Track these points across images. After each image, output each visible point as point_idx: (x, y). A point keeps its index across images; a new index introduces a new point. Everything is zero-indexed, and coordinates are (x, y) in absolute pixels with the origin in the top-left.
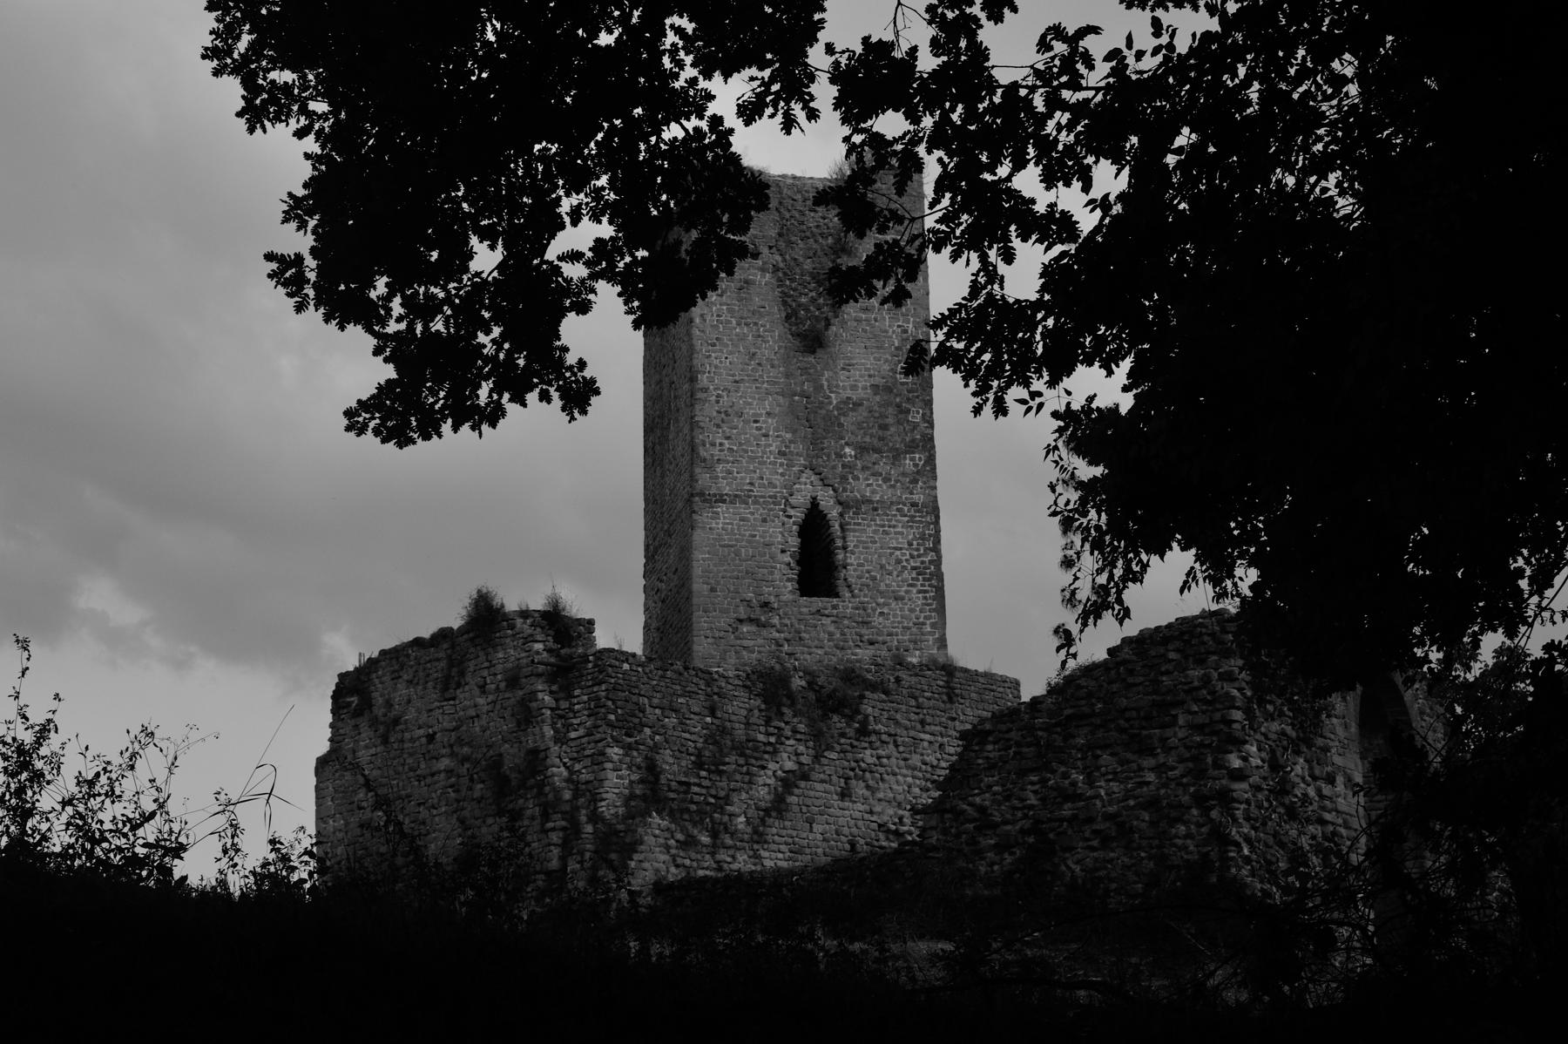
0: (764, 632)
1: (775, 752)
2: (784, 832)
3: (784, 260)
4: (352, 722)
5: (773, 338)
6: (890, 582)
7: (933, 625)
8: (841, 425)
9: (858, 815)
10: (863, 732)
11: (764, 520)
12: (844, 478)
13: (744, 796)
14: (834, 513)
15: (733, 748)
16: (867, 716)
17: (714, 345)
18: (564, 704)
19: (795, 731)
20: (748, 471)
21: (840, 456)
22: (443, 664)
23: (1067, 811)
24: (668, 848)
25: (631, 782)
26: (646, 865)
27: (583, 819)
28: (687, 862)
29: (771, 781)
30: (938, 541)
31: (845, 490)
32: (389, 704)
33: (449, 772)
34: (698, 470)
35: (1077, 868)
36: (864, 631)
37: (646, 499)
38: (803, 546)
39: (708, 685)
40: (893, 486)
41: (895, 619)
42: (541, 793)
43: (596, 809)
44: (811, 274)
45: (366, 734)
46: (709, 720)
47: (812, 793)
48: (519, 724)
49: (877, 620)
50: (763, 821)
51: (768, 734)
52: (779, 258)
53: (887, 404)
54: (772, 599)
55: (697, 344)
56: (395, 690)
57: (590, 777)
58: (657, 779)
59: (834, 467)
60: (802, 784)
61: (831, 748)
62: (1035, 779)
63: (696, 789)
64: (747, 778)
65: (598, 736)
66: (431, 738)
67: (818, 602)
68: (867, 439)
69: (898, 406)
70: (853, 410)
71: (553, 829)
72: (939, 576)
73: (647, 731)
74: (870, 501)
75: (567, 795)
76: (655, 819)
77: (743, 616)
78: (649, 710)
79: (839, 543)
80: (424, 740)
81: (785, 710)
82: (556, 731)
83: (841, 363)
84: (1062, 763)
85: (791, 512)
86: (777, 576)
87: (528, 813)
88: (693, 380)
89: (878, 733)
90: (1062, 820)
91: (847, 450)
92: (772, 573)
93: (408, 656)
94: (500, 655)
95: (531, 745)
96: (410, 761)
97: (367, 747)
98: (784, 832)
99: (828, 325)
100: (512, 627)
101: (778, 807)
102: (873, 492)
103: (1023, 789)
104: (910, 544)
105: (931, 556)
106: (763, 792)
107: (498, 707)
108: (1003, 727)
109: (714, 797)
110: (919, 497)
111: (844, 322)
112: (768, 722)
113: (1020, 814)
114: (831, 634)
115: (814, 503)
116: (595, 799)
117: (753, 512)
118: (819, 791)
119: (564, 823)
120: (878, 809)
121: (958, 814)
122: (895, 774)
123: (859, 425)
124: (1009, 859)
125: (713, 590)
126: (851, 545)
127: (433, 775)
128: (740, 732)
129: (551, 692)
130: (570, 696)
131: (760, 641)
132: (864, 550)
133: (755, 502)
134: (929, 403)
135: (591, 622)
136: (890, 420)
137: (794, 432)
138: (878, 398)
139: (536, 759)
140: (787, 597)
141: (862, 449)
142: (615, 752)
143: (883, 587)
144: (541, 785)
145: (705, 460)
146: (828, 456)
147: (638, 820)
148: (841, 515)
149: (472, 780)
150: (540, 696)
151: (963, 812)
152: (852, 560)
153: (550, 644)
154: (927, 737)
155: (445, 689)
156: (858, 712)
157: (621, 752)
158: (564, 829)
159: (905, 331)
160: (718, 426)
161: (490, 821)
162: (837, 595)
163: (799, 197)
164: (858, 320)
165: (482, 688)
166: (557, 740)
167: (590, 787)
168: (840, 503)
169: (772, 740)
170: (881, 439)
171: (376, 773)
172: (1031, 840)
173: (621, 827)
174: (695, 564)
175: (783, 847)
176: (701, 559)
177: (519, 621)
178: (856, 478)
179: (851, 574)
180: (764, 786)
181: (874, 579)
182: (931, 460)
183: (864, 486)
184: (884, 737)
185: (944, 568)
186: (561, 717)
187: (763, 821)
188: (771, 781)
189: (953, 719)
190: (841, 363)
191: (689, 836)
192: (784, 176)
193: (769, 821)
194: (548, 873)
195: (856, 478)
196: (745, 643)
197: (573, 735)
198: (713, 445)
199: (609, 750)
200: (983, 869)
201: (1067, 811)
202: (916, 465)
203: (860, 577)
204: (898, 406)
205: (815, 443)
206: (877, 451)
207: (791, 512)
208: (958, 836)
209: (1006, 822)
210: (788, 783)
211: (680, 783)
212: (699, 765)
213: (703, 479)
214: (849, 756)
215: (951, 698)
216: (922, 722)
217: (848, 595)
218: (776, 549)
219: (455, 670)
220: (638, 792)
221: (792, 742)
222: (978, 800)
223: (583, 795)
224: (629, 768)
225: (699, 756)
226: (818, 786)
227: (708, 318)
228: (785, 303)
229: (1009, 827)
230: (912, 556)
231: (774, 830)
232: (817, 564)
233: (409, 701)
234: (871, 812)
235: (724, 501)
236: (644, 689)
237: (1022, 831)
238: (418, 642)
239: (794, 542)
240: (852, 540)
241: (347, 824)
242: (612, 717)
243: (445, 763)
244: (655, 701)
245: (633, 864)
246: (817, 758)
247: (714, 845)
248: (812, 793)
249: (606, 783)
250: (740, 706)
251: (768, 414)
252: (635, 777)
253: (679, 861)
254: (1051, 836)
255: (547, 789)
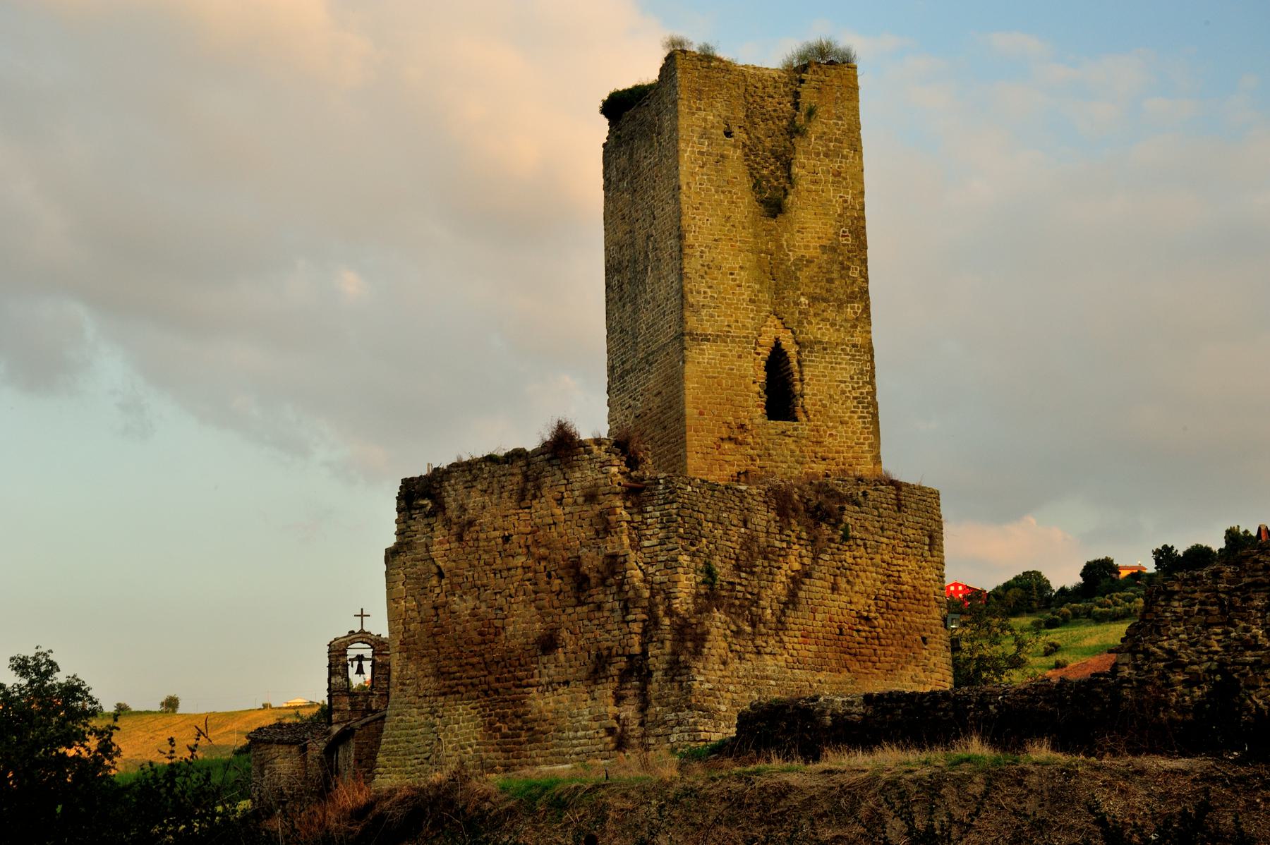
0: (741, 449)
1: (785, 556)
2: (797, 621)
3: (750, 138)
4: (426, 521)
5: (745, 205)
6: (836, 409)
7: (871, 445)
8: (797, 279)
9: (843, 605)
10: (845, 538)
11: (740, 357)
12: (800, 323)
13: (769, 592)
14: (792, 351)
15: (760, 553)
16: (847, 525)
17: (697, 209)
18: (638, 518)
19: (799, 538)
20: (726, 315)
21: (797, 304)
22: (519, 478)
23: (1249, 657)
24: (725, 636)
25: (697, 584)
26: (713, 651)
27: (661, 613)
28: (738, 648)
29: (784, 579)
30: (873, 376)
31: (801, 332)
32: (463, 508)
33: (526, 568)
34: (687, 314)
35: (1261, 703)
36: (818, 449)
37: (610, 330)
38: (769, 378)
39: (741, 502)
40: (838, 330)
41: (842, 440)
42: (620, 589)
43: (670, 605)
44: (771, 151)
45: (440, 532)
46: (743, 530)
47: (814, 589)
48: (597, 532)
49: (828, 441)
50: (783, 612)
51: (782, 541)
52: (745, 136)
53: (832, 262)
54: (747, 422)
55: (685, 207)
56: (468, 497)
57: (665, 579)
58: (714, 579)
59: (792, 313)
60: (807, 581)
61: (825, 552)
62: (1219, 631)
63: (739, 588)
64: (770, 578)
65: (670, 546)
66: (506, 539)
67: (783, 425)
68: (818, 291)
69: (841, 263)
70: (806, 266)
71: (635, 621)
72: (875, 406)
73: (704, 540)
74: (820, 342)
75: (647, 594)
76: (718, 615)
77: (725, 436)
78: (705, 524)
79: (797, 376)
80: (500, 541)
81: (793, 521)
82: (632, 540)
83: (796, 227)
84: (1242, 619)
85: (760, 350)
86: (751, 403)
87: (608, 606)
88: (681, 237)
89: (854, 538)
90: (1244, 664)
91: (803, 299)
92: (746, 400)
93: (481, 469)
94: (578, 475)
95: (610, 551)
96: (485, 556)
97: (441, 543)
98: (797, 621)
99: (786, 194)
100: (590, 452)
101: (792, 600)
102: (823, 335)
103: (1208, 638)
104: (852, 378)
105: (868, 388)
106: (779, 587)
107: (576, 517)
108: (1188, 589)
109: (751, 594)
110: (858, 340)
111: (798, 192)
112: (781, 532)
113: (1205, 658)
114: (793, 452)
115: (777, 343)
116: (669, 597)
117: (731, 350)
118: (816, 587)
119: (644, 616)
120: (855, 600)
121: (1148, 655)
122: (865, 571)
123: (811, 279)
124: (1198, 692)
125: (701, 414)
126: (807, 378)
127: (509, 569)
128: (762, 539)
129: (626, 508)
130: (641, 512)
131: (739, 457)
132: (817, 382)
133: (733, 342)
134: (864, 262)
135: (561, 427)
136: (835, 275)
137: (761, 283)
138: (825, 257)
139: (614, 563)
140: (758, 421)
141: (814, 299)
142: (684, 559)
143: (831, 414)
144: (620, 585)
145: (692, 306)
146: (788, 304)
147: (705, 615)
148: (798, 353)
149: (549, 576)
150: (618, 510)
151: (1154, 653)
152: (807, 390)
153: (624, 468)
154: (885, 540)
155: (522, 498)
156: (841, 521)
157: (688, 558)
158: (644, 621)
159: (846, 201)
160: (702, 277)
161: (570, 610)
162: (796, 419)
163: (759, 85)
164: (809, 191)
165: (560, 501)
166: (633, 547)
167: (664, 586)
168: (797, 343)
169: (784, 545)
170: (828, 291)
171: (450, 565)
172: (1218, 678)
173: (693, 621)
174: (687, 392)
175: (798, 634)
176: (692, 388)
177: (595, 448)
178: (810, 323)
179: (808, 401)
180: (779, 588)
181: (824, 406)
182: (867, 309)
183: (815, 330)
184: (859, 542)
185: (878, 398)
186: (634, 528)
187: (783, 612)
188: (784, 579)
189: (900, 525)
190: (796, 227)
191: (738, 626)
192: (746, 66)
193: (788, 612)
194: (631, 657)
195: (810, 323)
196: (728, 458)
197: (646, 543)
198: (699, 292)
199: (680, 558)
200: (1174, 699)
201: (1249, 657)
202: (855, 313)
203: (814, 405)
204: (841, 263)
205: (778, 292)
206: (826, 300)
207: (760, 350)
208: (1150, 671)
209: (1194, 663)
210: (797, 581)
211: (729, 583)
212: (738, 567)
213: (691, 322)
214: (837, 557)
215: (900, 507)
216: (882, 528)
217: (805, 419)
218: (749, 381)
219: (530, 485)
220: (703, 592)
221: (796, 547)
222: (1166, 644)
223: (658, 593)
224: (695, 572)
225: (737, 560)
226: (818, 583)
227: (693, 186)
228: (751, 175)
229: (1195, 667)
230: (853, 388)
231: (791, 620)
232: (781, 396)
233: (484, 508)
234: (851, 603)
235: (708, 340)
236: (702, 506)
237: (1209, 671)
238: (491, 459)
239: (762, 374)
240: (807, 373)
241: (420, 605)
242: (681, 530)
243: (520, 560)
244: (709, 516)
245: (706, 651)
246: (815, 559)
247: (754, 634)
248: (814, 589)
249: (680, 585)
250: (763, 518)
251: (741, 268)
252: (699, 579)
253: (734, 647)
254: (1236, 676)
255: (627, 588)
